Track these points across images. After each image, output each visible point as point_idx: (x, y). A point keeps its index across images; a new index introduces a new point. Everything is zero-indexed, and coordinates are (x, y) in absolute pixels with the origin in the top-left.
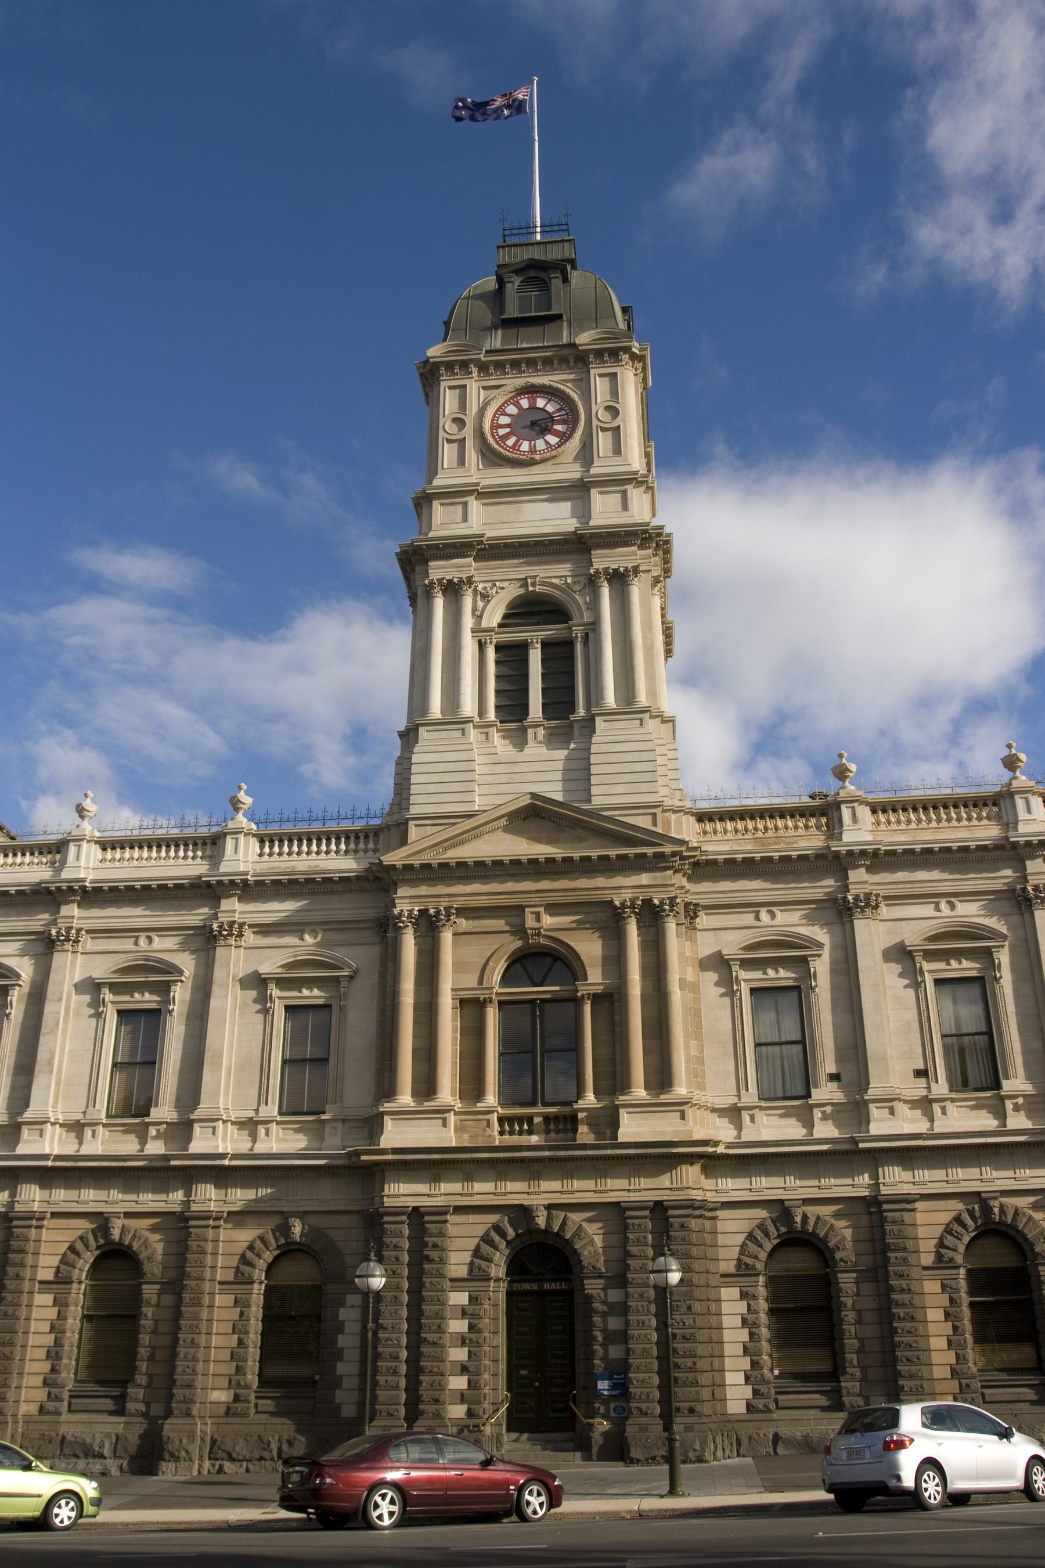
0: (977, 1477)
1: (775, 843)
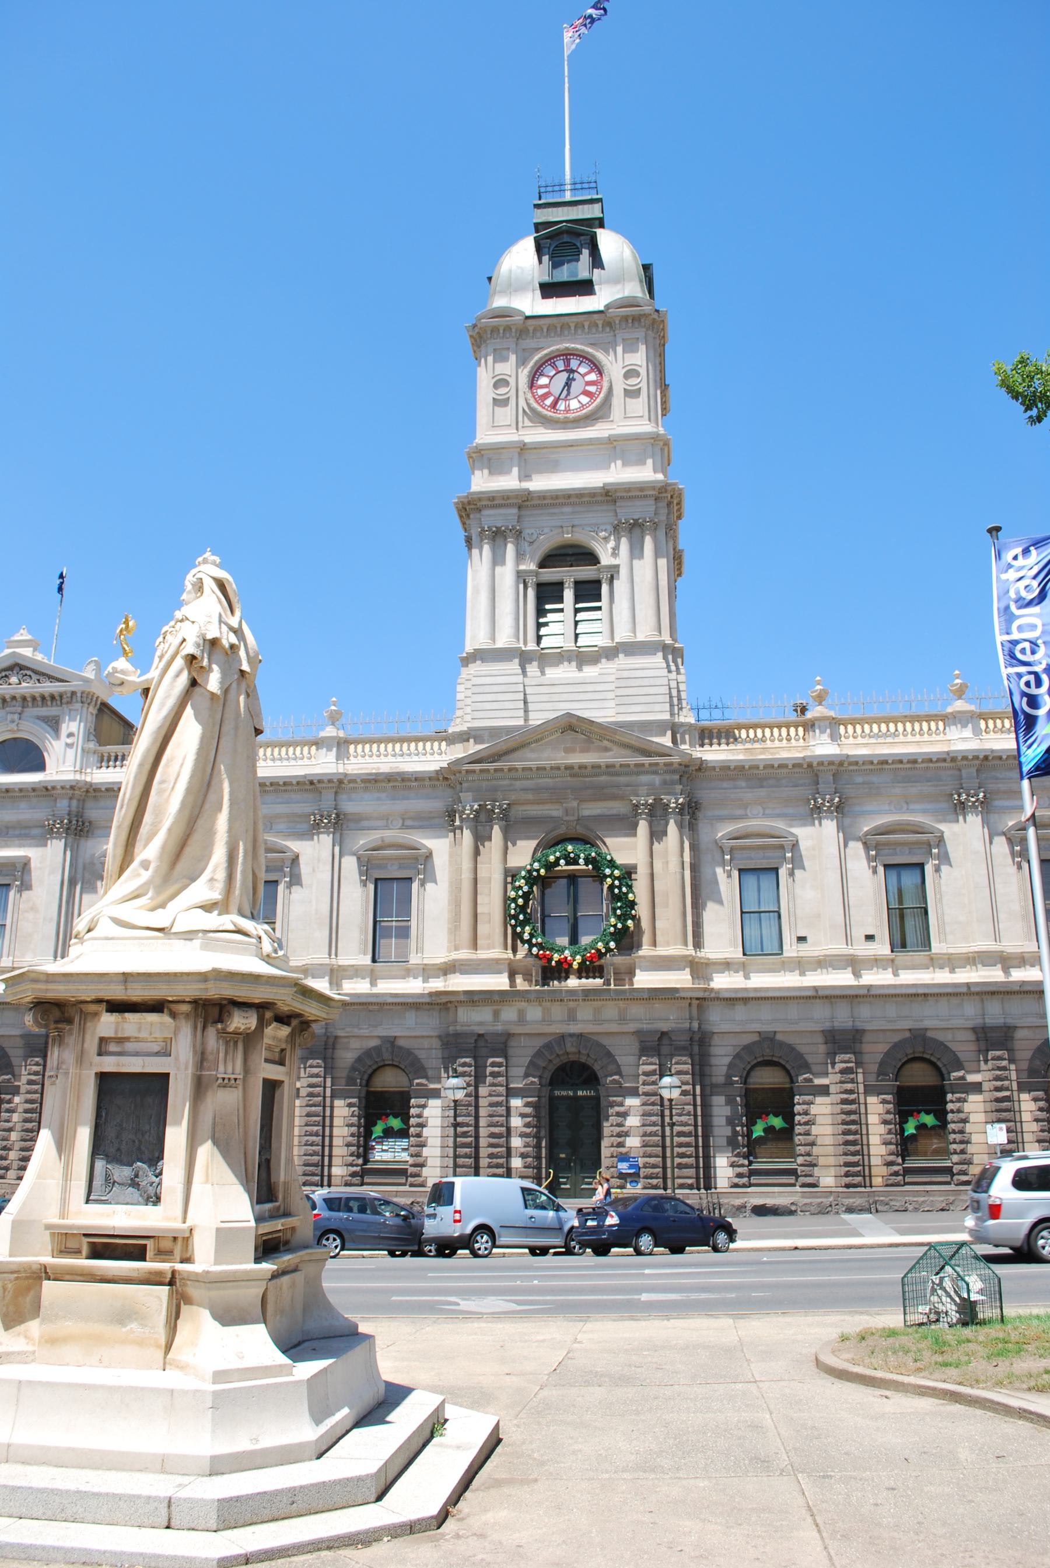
0: (367, 913)
1: (761, 754)
